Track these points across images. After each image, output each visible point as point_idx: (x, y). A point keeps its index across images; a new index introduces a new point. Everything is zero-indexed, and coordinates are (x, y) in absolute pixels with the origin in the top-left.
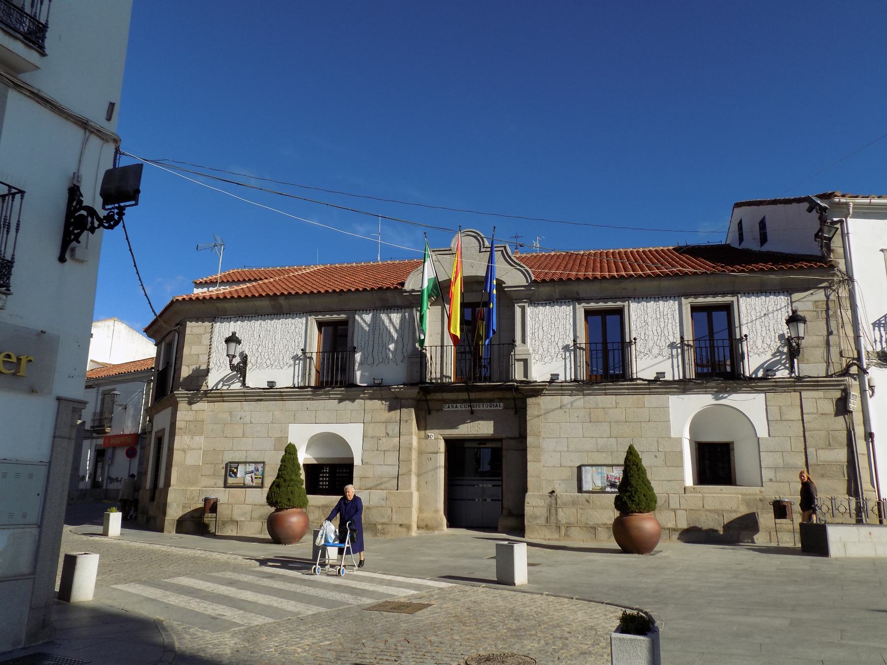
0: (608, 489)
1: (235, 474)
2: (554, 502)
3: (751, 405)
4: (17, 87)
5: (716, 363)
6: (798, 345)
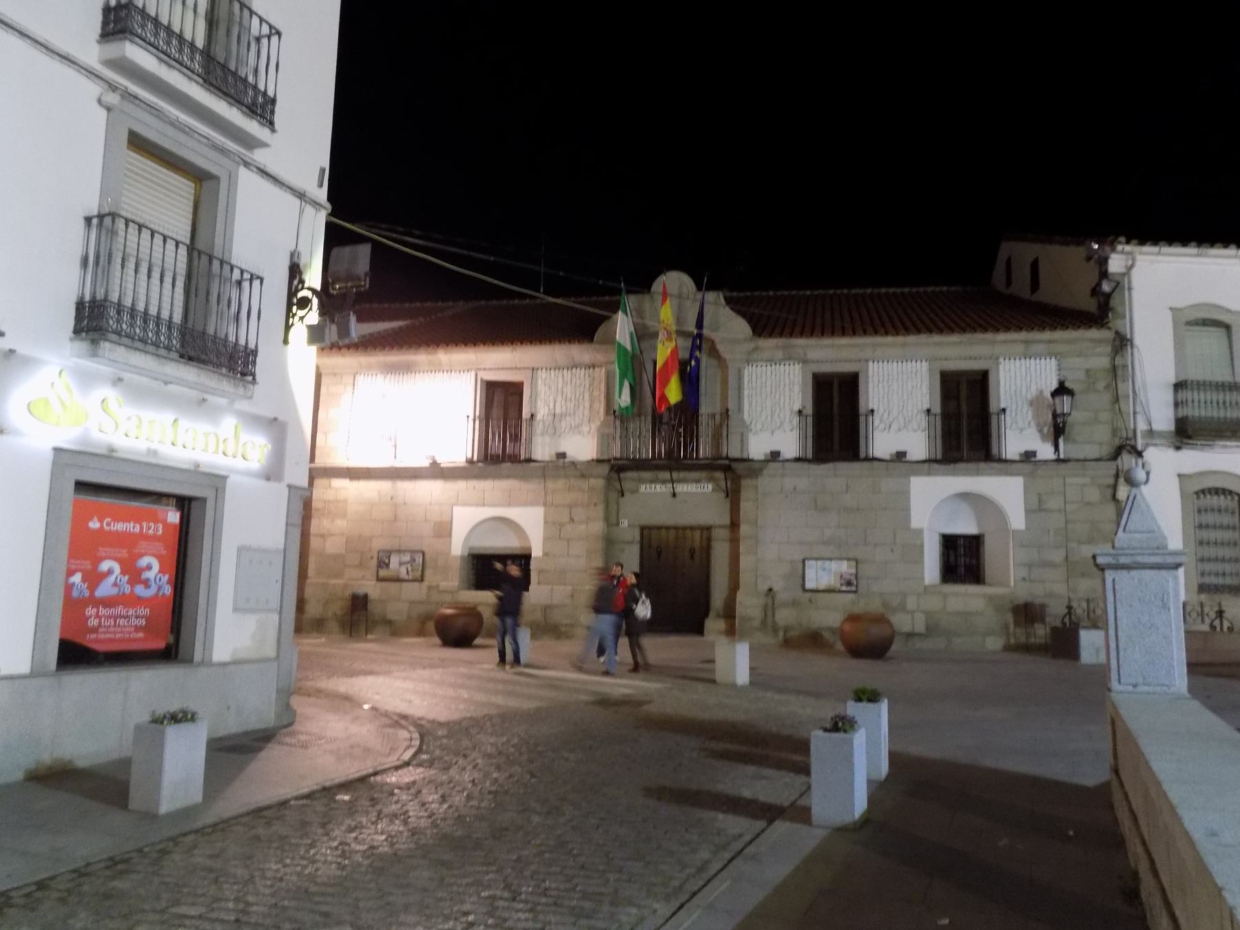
0: (844, 588)
1: (387, 565)
2: (770, 601)
3: (1007, 492)
4: (247, 164)
5: (966, 424)
6: (1064, 423)
